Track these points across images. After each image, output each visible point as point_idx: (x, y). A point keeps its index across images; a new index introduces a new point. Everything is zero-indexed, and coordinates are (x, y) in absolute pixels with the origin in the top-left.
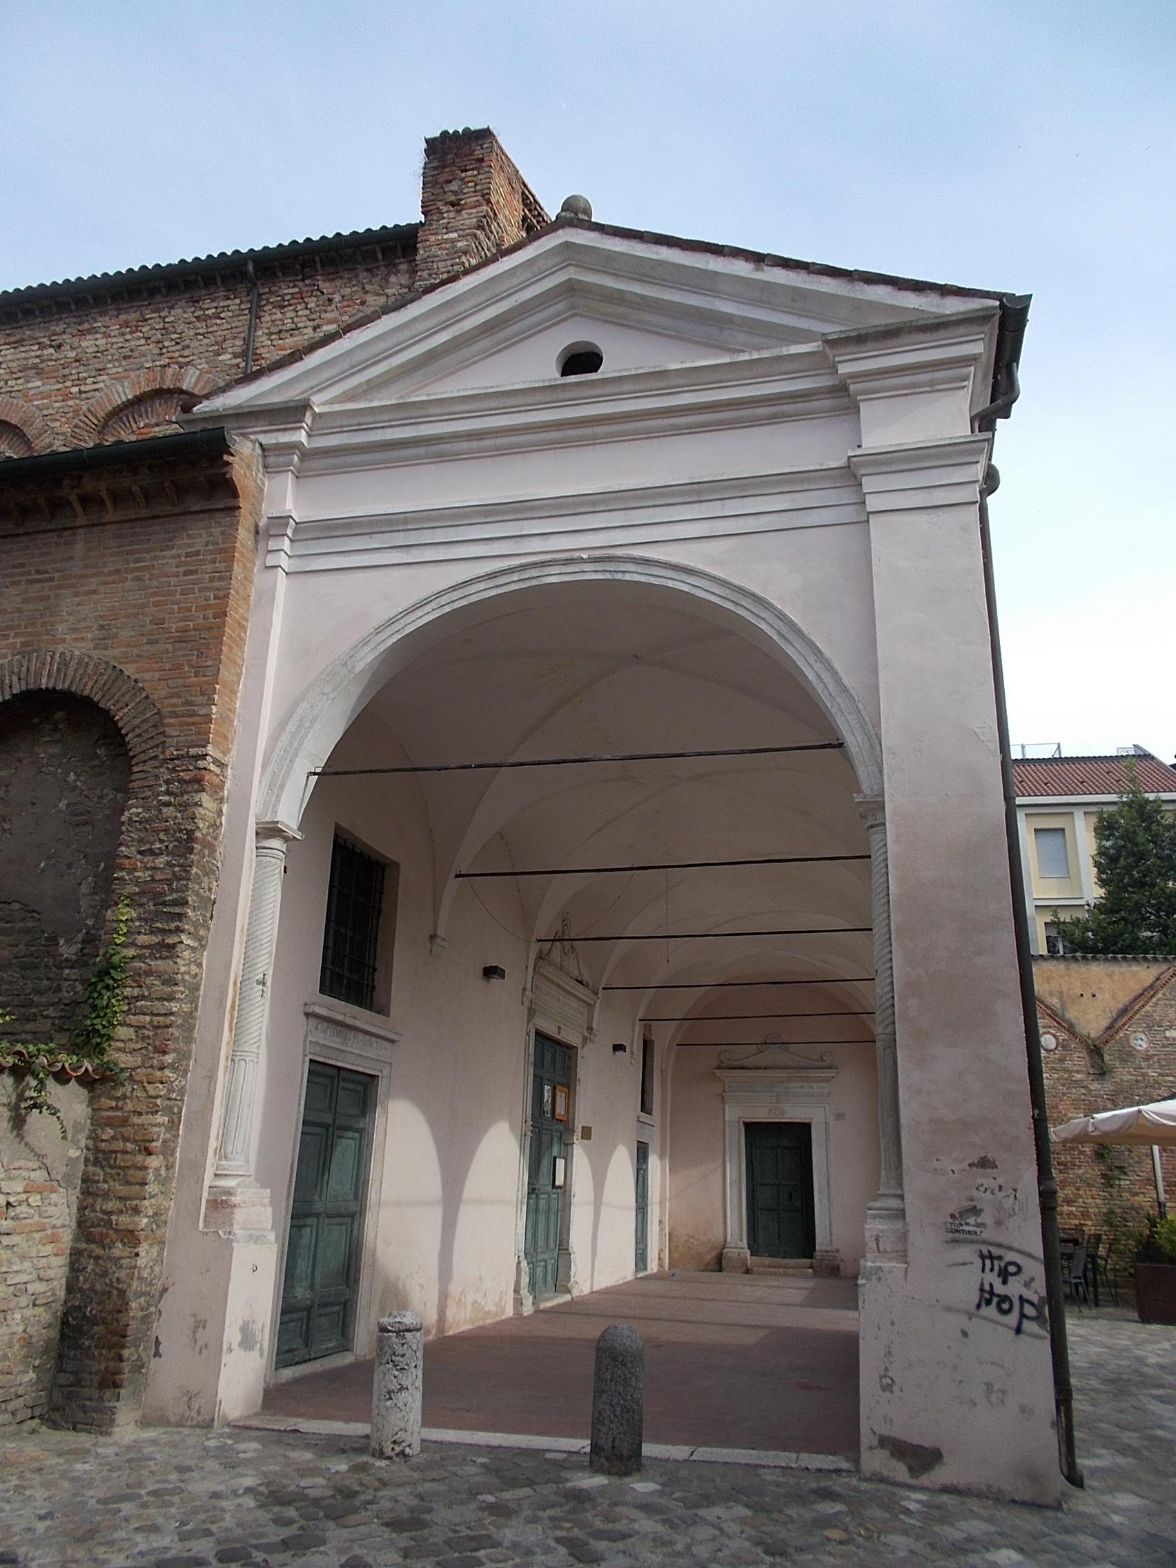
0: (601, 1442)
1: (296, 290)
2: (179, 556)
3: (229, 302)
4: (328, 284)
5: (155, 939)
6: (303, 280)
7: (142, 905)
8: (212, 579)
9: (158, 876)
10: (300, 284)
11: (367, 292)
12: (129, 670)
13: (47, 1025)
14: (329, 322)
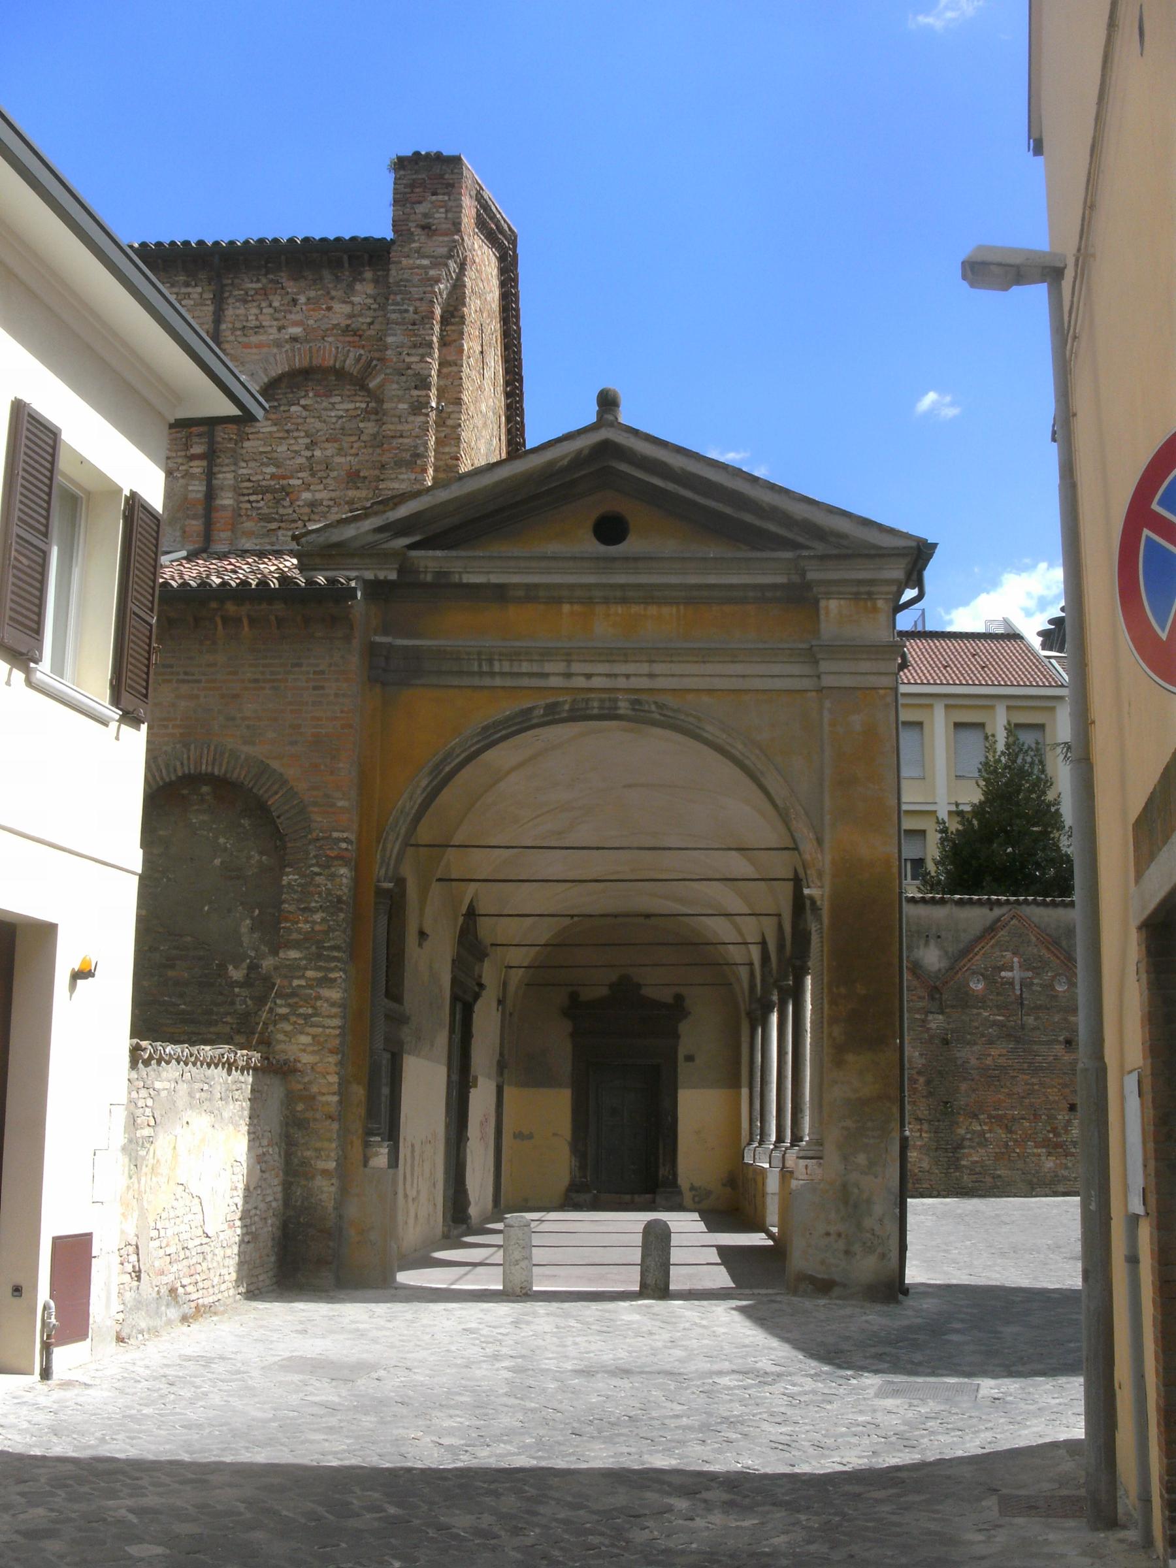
0: (648, 1282)
1: (259, 285)
2: (308, 673)
3: (189, 290)
4: (291, 284)
5: (320, 975)
6: (266, 275)
7: (307, 948)
8: (336, 695)
9: (317, 928)
10: (264, 280)
11: (332, 298)
12: (275, 764)
13: (227, 1029)
14: (296, 324)
